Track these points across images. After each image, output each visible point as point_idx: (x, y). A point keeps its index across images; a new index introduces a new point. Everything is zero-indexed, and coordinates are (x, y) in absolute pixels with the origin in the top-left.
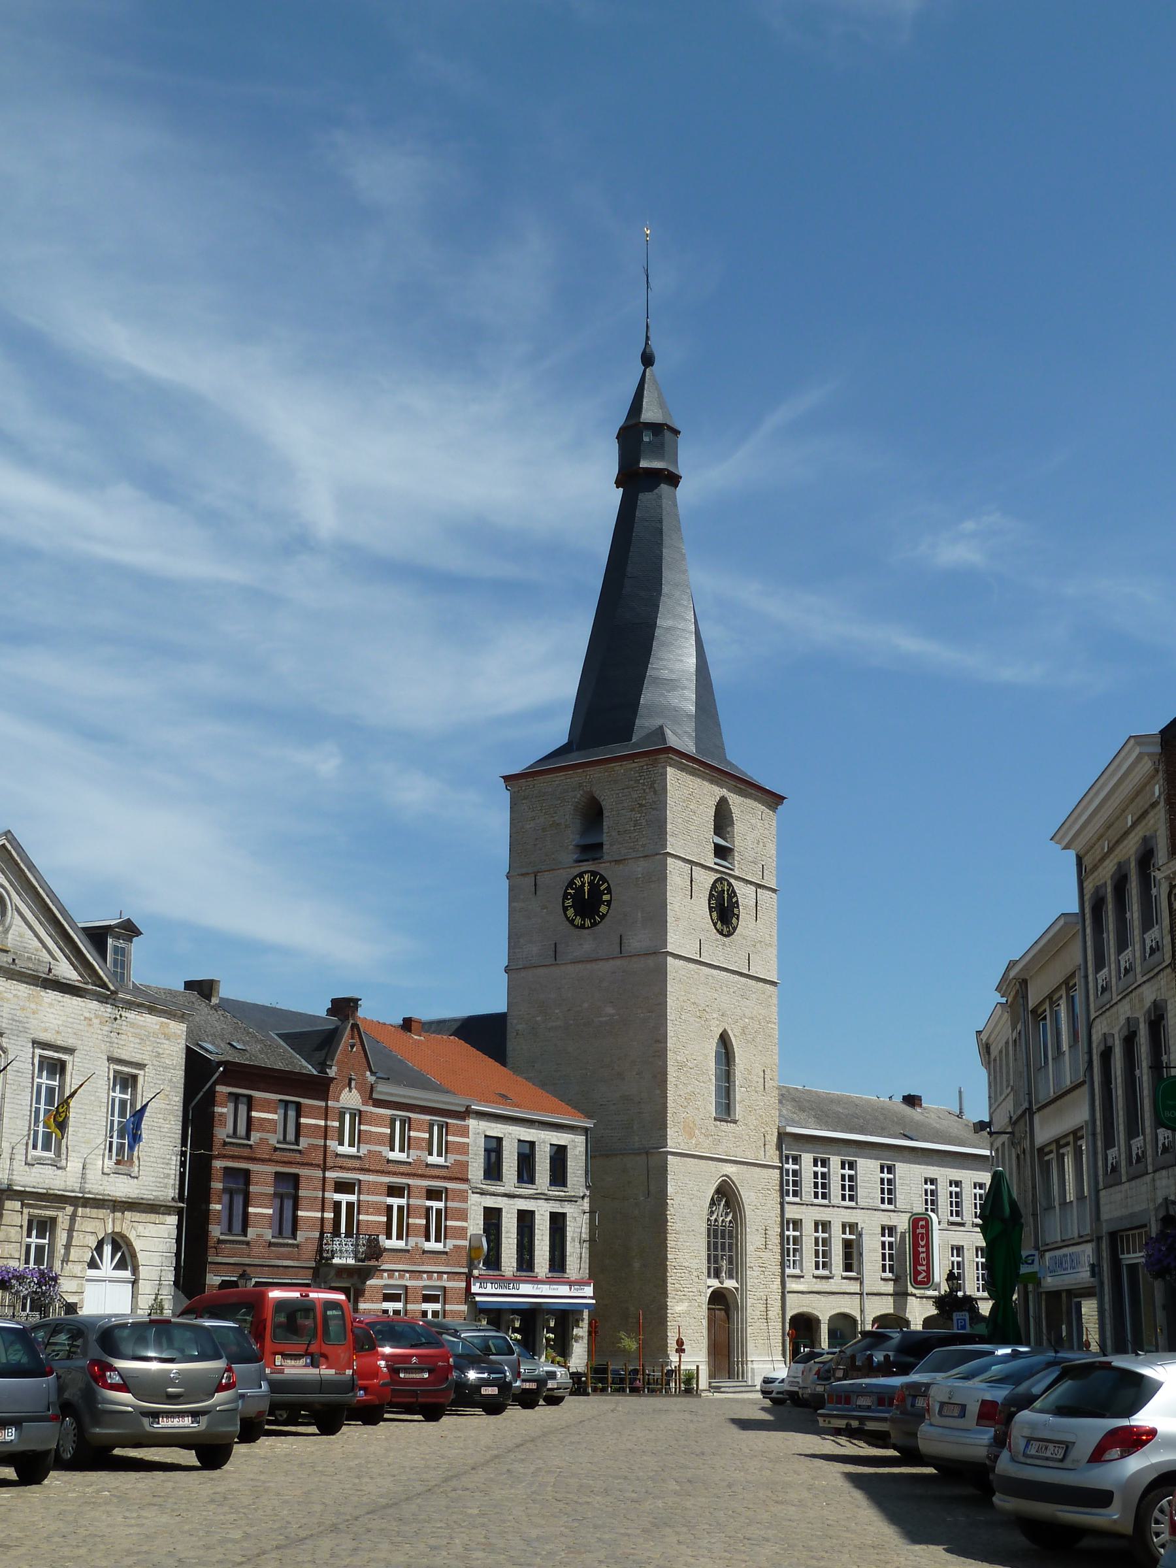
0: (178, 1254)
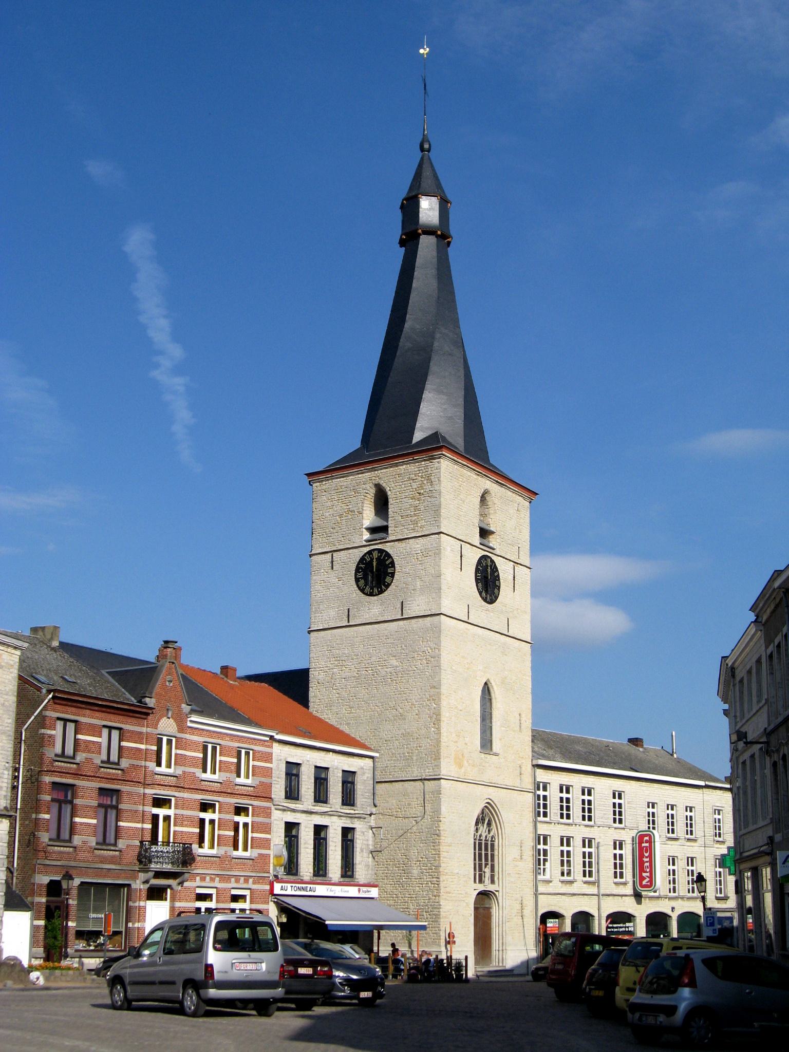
0: (10, 856)
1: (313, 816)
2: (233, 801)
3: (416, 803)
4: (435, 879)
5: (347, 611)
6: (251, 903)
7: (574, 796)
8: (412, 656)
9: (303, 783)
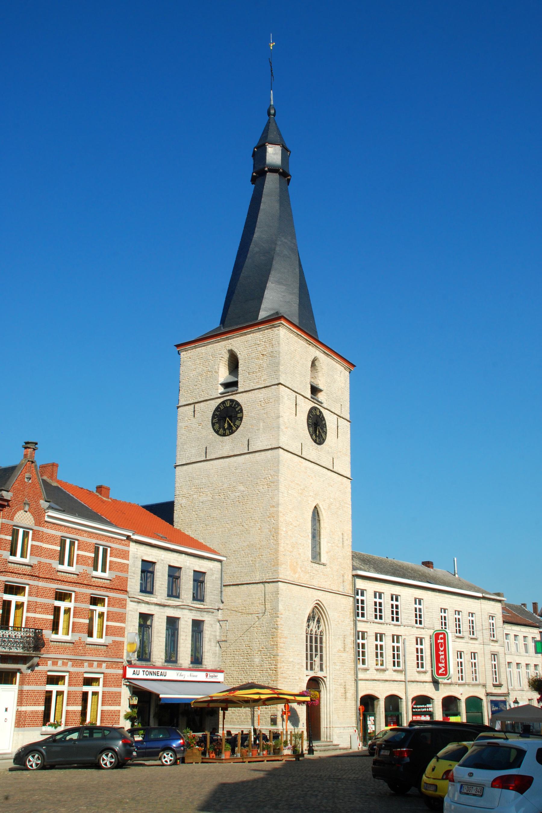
1: (166, 608)
2: (89, 591)
3: (258, 602)
4: (273, 666)
5: (205, 449)
6: (103, 687)
7: (386, 601)
8: (256, 483)
9: (157, 579)
